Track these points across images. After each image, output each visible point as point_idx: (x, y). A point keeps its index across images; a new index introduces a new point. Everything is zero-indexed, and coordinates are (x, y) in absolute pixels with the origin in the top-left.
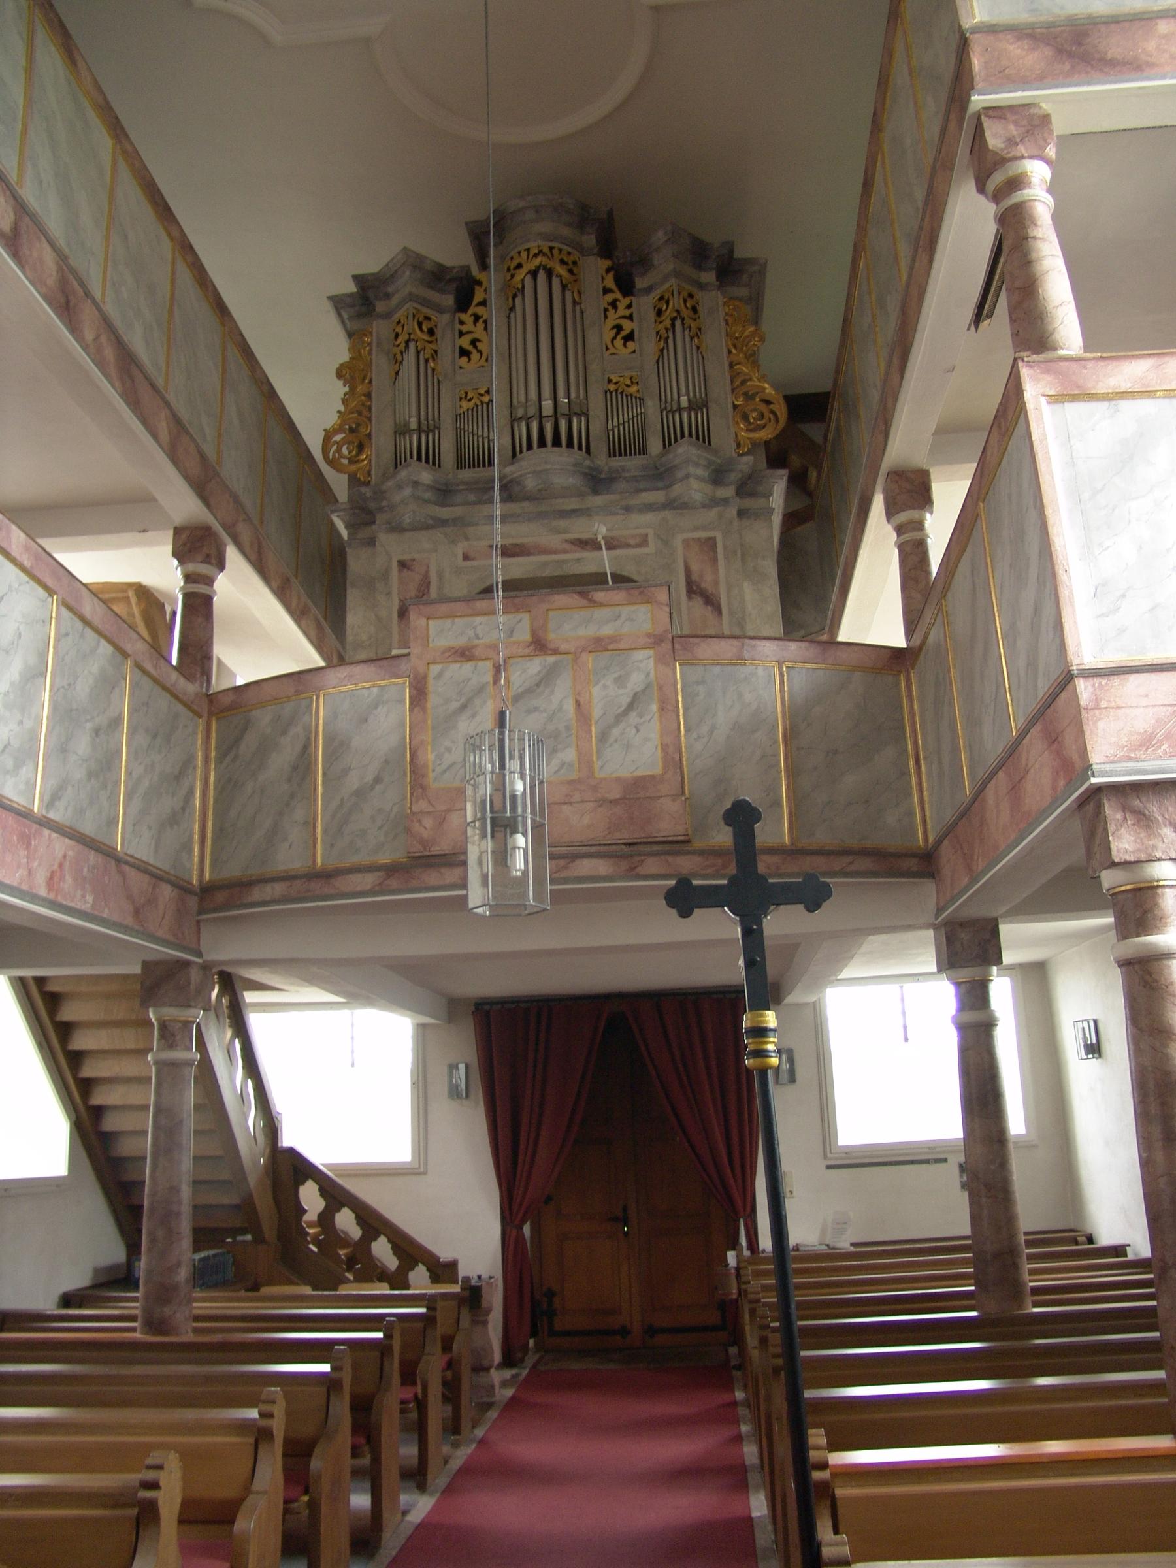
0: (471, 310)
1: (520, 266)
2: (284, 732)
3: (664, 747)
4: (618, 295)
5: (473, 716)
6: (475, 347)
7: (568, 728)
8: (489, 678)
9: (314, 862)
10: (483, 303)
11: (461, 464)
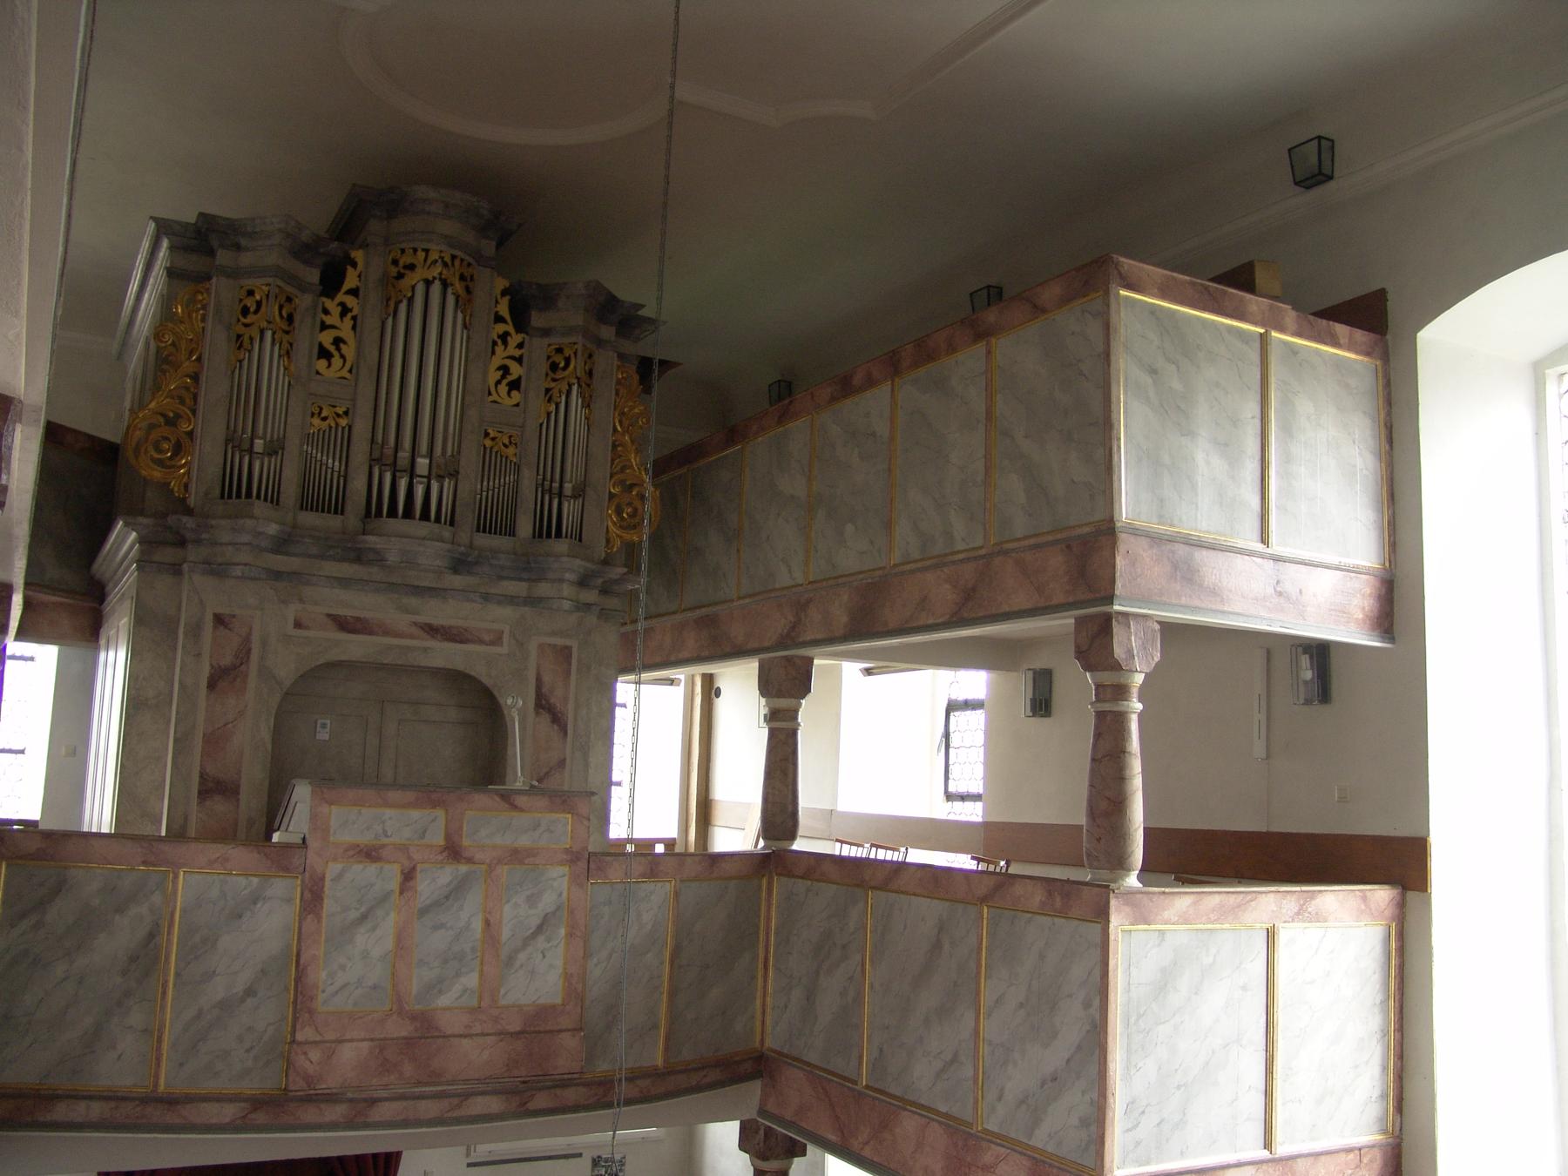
0: (340, 297)
1: (412, 267)
2: (120, 910)
3: (567, 977)
4: (510, 328)
5: (374, 929)
6: (338, 349)
7: (473, 949)
8: (394, 884)
9: (156, 1085)
10: (354, 292)
11: (306, 504)
